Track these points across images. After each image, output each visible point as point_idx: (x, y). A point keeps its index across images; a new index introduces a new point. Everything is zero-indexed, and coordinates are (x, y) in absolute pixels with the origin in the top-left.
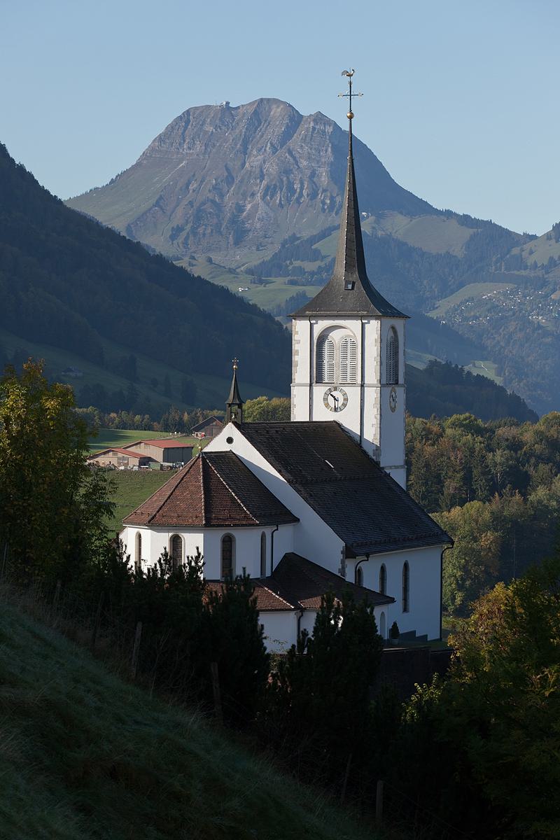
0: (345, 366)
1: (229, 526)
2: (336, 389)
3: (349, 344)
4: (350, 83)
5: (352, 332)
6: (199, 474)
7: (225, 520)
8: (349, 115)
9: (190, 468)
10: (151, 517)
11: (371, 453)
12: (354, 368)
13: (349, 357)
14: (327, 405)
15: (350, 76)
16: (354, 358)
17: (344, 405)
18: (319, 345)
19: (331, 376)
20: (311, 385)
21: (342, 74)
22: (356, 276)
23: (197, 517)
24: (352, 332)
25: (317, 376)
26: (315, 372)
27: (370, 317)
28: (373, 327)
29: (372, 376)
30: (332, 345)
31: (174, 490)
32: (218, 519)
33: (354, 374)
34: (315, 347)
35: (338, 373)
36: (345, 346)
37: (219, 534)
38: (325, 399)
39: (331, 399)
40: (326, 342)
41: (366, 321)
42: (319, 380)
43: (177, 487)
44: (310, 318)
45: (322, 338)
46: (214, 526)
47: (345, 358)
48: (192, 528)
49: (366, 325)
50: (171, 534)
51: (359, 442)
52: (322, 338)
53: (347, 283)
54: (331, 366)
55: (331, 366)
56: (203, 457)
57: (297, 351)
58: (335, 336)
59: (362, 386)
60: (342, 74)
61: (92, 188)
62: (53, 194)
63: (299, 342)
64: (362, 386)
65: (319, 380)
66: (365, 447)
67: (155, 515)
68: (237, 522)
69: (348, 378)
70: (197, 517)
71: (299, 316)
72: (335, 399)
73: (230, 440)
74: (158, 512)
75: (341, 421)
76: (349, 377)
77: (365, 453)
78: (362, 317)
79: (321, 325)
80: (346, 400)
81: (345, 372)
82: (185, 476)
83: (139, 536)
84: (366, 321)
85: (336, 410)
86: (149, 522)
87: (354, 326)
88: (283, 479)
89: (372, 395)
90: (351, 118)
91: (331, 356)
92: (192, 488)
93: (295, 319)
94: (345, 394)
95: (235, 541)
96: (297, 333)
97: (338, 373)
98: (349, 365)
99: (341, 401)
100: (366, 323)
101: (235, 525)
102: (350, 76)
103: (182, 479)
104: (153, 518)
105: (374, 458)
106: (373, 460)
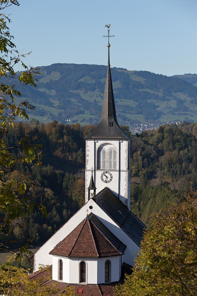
0: (111, 162)
1: (109, 256)
2: (107, 172)
3: (112, 152)
4: (109, 31)
5: (115, 146)
6: (89, 229)
7: (107, 253)
8: (108, 45)
9: (84, 226)
10: (69, 253)
11: (123, 202)
12: (115, 162)
13: (112, 158)
14: (102, 180)
15: (109, 27)
16: (115, 158)
17: (111, 180)
18: (98, 152)
19: (104, 166)
20: (95, 171)
21: (105, 26)
22: (113, 120)
23: (93, 253)
24: (115, 146)
25: (98, 167)
26: (96, 165)
27: (123, 139)
28: (125, 144)
29: (124, 166)
30: (104, 152)
31: (78, 238)
32: (104, 253)
33: (115, 165)
34: (97, 153)
35: (107, 165)
36: (111, 152)
37: (104, 260)
38: (102, 177)
39: (104, 178)
40: (102, 151)
41: (121, 141)
42: (99, 168)
43: (79, 236)
44: (94, 139)
45: (100, 149)
46: (102, 257)
47: (110, 158)
48: (92, 258)
49: (121, 143)
50: (80, 261)
51: (118, 197)
52: (100, 149)
53: (109, 123)
54: (104, 162)
55: (104, 162)
56: (89, 220)
57: (88, 155)
58: (106, 148)
59: (120, 171)
60: (105, 26)
61: (154, 73)
62: (164, 75)
63: (89, 151)
64: (120, 171)
65: (99, 168)
66: (121, 199)
67: (71, 251)
68: (112, 254)
69: (112, 167)
70: (93, 253)
71: (89, 139)
72: (106, 177)
73: (91, 207)
74: (72, 250)
75: (109, 187)
76: (112, 167)
77: (121, 202)
78: (119, 139)
79: (99, 143)
80: (112, 177)
81: (110, 165)
82: (82, 230)
83: (61, 262)
84: (121, 141)
85: (106, 182)
86: (69, 255)
87: (115, 143)
88: (119, 227)
89: (124, 175)
90: (109, 47)
91: (104, 158)
92: (87, 237)
93: (87, 140)
94: (111, 175)
95: (111, 263)
96: (88, 146)
97: (107, 165)
98: (112, 162)
99: (109, 179)
100: (121, 142)
101: (112, 256)
102: (109, 27)
103: (81, 232)
104: (70, 253)
105: (125, 204)
106: (125, 205)
